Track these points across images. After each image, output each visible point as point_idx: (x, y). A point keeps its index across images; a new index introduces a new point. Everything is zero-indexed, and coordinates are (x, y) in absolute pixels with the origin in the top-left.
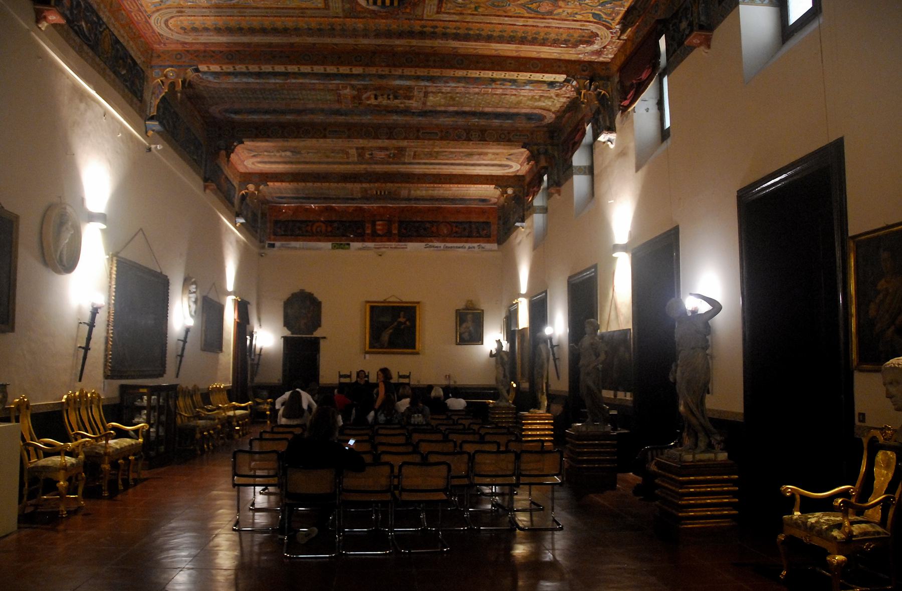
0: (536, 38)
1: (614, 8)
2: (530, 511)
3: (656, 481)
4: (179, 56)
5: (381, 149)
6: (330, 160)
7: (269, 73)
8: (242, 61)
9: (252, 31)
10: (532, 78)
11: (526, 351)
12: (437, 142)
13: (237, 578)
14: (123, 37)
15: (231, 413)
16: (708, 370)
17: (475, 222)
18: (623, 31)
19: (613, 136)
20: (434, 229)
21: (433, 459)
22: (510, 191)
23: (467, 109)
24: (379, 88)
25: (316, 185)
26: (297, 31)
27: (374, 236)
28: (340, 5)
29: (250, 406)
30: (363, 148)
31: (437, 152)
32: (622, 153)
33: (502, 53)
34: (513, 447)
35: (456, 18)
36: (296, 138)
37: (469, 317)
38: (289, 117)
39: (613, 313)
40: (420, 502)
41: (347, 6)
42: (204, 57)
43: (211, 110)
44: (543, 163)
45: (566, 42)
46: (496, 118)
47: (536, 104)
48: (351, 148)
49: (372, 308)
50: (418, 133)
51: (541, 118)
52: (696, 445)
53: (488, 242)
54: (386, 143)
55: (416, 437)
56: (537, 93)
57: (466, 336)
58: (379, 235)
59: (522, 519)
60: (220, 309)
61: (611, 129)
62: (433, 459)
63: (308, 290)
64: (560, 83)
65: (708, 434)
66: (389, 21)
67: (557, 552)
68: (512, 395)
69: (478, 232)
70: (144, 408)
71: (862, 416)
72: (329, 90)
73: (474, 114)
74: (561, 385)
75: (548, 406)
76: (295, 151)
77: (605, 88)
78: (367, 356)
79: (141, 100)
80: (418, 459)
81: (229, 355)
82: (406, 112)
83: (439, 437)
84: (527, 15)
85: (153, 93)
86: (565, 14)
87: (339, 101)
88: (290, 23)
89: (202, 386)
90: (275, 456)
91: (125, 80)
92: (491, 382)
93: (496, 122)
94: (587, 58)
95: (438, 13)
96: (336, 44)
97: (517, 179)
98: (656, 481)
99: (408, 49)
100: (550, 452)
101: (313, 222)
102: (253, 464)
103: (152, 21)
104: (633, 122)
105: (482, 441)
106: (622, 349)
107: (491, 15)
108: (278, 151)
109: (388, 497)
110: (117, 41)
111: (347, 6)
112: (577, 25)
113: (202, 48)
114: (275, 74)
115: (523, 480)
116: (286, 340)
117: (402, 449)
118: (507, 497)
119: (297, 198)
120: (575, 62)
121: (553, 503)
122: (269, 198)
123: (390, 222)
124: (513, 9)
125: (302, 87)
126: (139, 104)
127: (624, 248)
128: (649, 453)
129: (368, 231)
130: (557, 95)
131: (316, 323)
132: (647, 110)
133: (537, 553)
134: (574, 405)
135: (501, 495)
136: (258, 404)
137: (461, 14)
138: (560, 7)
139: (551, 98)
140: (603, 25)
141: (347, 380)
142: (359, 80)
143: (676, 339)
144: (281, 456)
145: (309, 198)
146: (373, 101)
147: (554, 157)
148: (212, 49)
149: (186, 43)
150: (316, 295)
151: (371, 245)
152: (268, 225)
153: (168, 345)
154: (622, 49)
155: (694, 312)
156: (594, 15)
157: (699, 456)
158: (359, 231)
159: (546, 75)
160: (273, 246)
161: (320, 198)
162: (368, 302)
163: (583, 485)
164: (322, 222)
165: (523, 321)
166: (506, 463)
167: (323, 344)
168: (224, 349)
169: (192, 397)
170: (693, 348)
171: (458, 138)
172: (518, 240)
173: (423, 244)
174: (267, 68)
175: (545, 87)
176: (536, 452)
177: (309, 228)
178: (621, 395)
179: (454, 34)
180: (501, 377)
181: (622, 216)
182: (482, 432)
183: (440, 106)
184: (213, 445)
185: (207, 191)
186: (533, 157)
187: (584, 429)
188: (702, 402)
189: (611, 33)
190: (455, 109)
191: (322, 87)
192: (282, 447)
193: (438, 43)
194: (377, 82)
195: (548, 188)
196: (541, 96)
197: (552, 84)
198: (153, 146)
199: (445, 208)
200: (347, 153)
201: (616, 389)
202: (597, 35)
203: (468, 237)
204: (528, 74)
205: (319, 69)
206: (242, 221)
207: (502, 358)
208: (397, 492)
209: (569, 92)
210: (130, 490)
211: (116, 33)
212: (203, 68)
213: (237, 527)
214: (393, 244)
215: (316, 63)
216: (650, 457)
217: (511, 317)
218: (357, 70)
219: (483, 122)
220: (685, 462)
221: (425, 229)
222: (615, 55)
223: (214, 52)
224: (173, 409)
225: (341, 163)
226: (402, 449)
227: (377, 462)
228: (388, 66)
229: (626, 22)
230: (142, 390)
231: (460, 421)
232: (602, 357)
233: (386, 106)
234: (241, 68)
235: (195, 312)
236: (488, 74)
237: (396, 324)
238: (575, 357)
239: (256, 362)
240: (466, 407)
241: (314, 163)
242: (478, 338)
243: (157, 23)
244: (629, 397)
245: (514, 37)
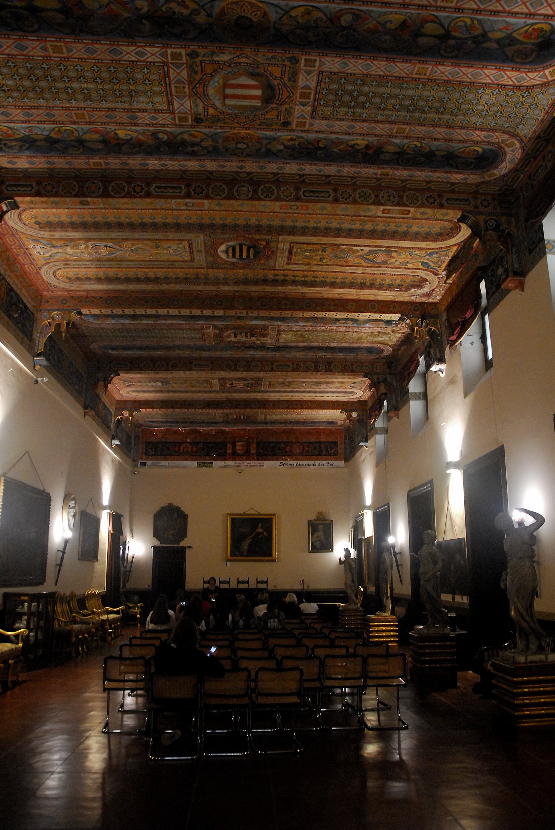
0: (374, 284)
1: (439, 258)
2: (377, 710)
3: (493, 692)
4: (64, 302)
5: (240, 379)
6: (194, 389)
7: (142, 315)
8: (119, 306)
9: (128, 280)
10: (371, 318)
11: (371, 561)
12: (290, 373)
13: (104, 783)
14: (17, 285)
15: (104, 617)
16: (534, 578)
17: (325, 442)
18: (448, 277)
19: (443, 367)
20: (288, 449)
21: (288, 664)
22: (354, 415)
23: (315, 344)
24: (238, 327)
25: (183, 410)
26: (167, 280)
27: (235, 456)
28: (204, 258)
29: (122, 610)
30: (224, 379)
31: (290, 382)
32: (452, 382)
33: (344, 297)
34: (361, 650)
35: (305, 268)
36: (165, 370)
37: (320, 527)
38: (159, 353)
39: (448, 524)
40: (275, 705)
41: (210, 259)
42: (86, 301)
43: (91, 347)
44: (383, 389)
45: (399, 286)
46: (340, 352)
47: (376, 339)
48: (213, 379)
49: (233, 519)
50: (272, 365)
51: (380, 351)
52: (527, 647)
53: (336, 459)
54: (245, 374)
55: (273, 642)
56: (376, 330)
57: (318, 544)
58: (239, 455)
59: (371, 719)
60: (97, 522)
61: (441, 360)
62: (288, 664)
63: (176, 503)
64: (396, 321)
65: (538, 637)
66: (246, 271)
67: (403, 752)
68: (360, 599)
69: (327, 451)
70: (24, 614)
72: (194, 329)
73: (320, 348)
74: (404, 589)
75: (393, 608)
76: (165, 382)
77: (435, 325)
78: (229, 563)
79: (31, 339)
80: (271, 664)
81: (104, 563)
82: (262, 347)
83: (293, 642)
84: (364, 264)
85: (41, 333)
86: (398, 263)
87: (203, 339)
88: (160, 273)
89: (79, 592)
90: (142, 661)
91: (18, 323)
92: (342, 586)
93: (341, 355)
94: (418, 300)
95: (288, 264)
96: (200, 291)
97: (360, 404)
98: (493, 681)
99: (262, 294)
100: (395, 655)
101: (180, 443)
102: (122, 667)
103: (42, 272)
104: (460, 354)
105: (333, 645)
106: (458, 556)
107: (333, 265)
108: (150, 382)
109: (246, 701)
110: (12, 290)
111: (210, 259)
112: (409, 272)
113: (85, 294)
114: (147, 316)
115: (370, 682)
116: (155, 548)
117: (259, 654)
118: (356, 697)
119: (167, 422)
120: (408, 303)
121: (398, 702)
122: (141, 422)
123: (248, 443)
124: (352, 259)
125: (171, 327)
126: (28, 342)
127: (456, 465)
128: (486, 653)
129: (229, 451)
130: (393, 332)
131: (183, 533)
132: (472, 344)
133: (385, 752)
134: (415, 608)
135: (351, 694)
136: (130, 608)
137: (309, 264)
138: (394, 258)
139: (388, 333)
140: (431, 272)
142: (221, 321)
143: (505, 549)
144: (147, 663)
145: (177, 422)
146: (233, 339)
147: (392, 384)
148: (94, 295)
149: (71, 291)
151: (232, 463)
152: (141, 445)
153: (49, 556)
154: (448, 291)
155: (521, 523)
156: (423, 263)
157: (531, 658)
158: (221, 451)
159: (383, 315)
160: (144, 464)
161: (186, 422)
162: (228, 514)
163: (427, 684)
164: (188, 442)
165: (369, 531)
166: (355, 666)
167: (188, 552)
168: (99, 558)
169: (69, 602)
170: (521, 558)
171: (307, 370)
172: (362, 458)
173: (278, 463)
174: (140, 311)
175: (383, 325)
176: (381, 656)
177: (177, 449)
178: (458, 598)
179: (302, 281)
180: (350, 582)
181: (454, 435)
182: (333, 636)
183: (292, 342)
184: (87, 648)
185: (87, 417)
186: (374, 385)
187: (425, 631)
188: (531, 606)
189: (439, 278)
190: (305, 344)
191: (188, 327)
192: (149, 652)
193: (289, 289)
194: (234, 322)
195: (388, 411)
196: (381, 332)
197: (388, 322)
198: (40, 379)
199: (297, 430)
200: (211, 383)
201: (453, 593)
202: (427, 280)
203: (319, 455)
204: (368, 314)
205: (186, 312)
206: (118, 443)
207: (350, 565)
208: (254, 696)
209: (403, 328)
210: (9, 693)
211: (11, 282)
212: (85, 311)
213: (107, 731)
214: (252, 463)
215: (183, 307)
216: (486, 657)
217: (358, 527)
218: (219, 313)
219: (329, 355)
220: (520, 663)
221: (279, 449)
222: (443, 297)
223: (94, 298)
224: (51, 614)
225: (205, 392)
226: (259, 654)
227: (236, 668)
228: (245, 309)
229: (451, 268)
230: (23, 598)
231: (312, 625)
232: (440, 565)
233: (245, 343)
234: (118, 311)
235: (73, 525)
236: (333, 315)
237: (254, 534)
238: (415, 564)
239: (128, 569)
240: (318, 611)
241: (180, 392)
242: (329, 547)
243: (47, 274)
244: (465, 600)
245: (355, 283)
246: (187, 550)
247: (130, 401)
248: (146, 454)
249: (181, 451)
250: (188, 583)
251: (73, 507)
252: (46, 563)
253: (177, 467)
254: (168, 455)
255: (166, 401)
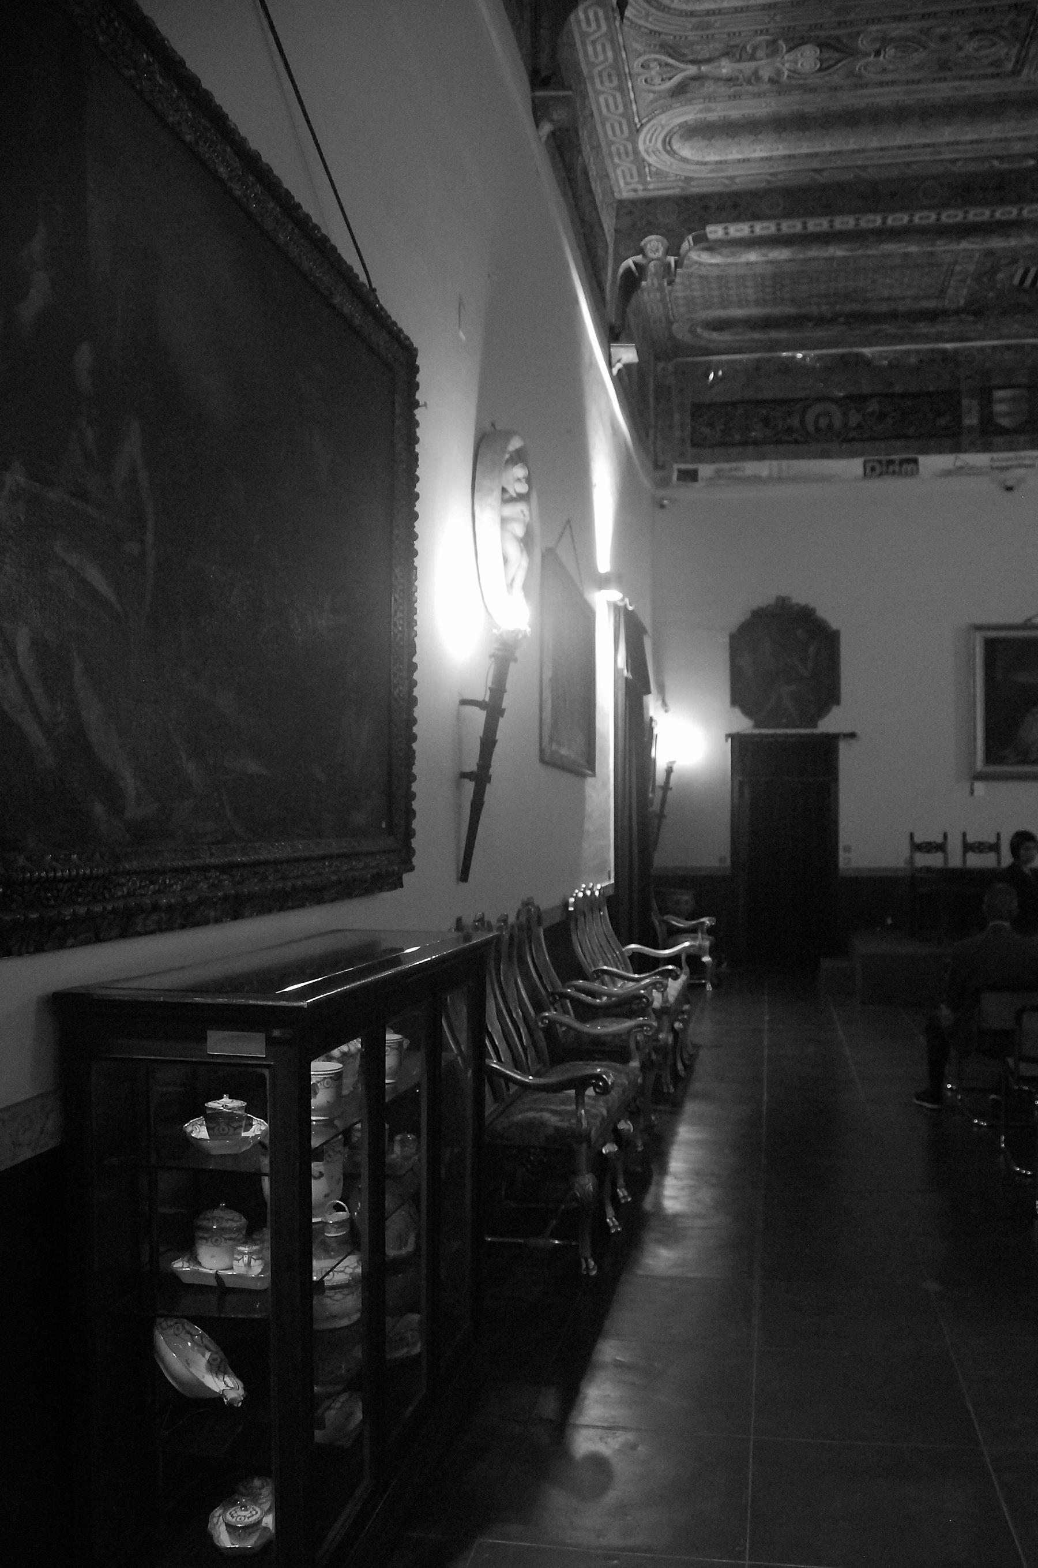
27: (990, 435)
49: (990, 645)
58: (1003, 431)
63: (800, 597)
71: (848, 849)
78: (980, 787)
81: (605, 785)
116: (740, 744)
129: (971, 420)
131: (825, 691)
141: (934, 860)
150: (821, 613)
152: (677, 416)
158: (942, 421)
160: (691, 476)
162: (978, 628)
164: (835, 401)
167: (847, 755)
177: (795, 422)
239: (655, 807)
246: (842, 745)
247: (668, 199)
248: (694, 445)
249: (811, 428)
250: (848, 849)
251: (521, 498)
252: (410, 757)
253: (795, 479)
254: (765, 442)
255: (805, 190)
